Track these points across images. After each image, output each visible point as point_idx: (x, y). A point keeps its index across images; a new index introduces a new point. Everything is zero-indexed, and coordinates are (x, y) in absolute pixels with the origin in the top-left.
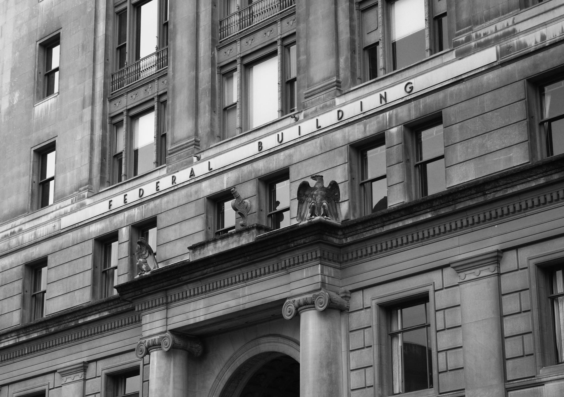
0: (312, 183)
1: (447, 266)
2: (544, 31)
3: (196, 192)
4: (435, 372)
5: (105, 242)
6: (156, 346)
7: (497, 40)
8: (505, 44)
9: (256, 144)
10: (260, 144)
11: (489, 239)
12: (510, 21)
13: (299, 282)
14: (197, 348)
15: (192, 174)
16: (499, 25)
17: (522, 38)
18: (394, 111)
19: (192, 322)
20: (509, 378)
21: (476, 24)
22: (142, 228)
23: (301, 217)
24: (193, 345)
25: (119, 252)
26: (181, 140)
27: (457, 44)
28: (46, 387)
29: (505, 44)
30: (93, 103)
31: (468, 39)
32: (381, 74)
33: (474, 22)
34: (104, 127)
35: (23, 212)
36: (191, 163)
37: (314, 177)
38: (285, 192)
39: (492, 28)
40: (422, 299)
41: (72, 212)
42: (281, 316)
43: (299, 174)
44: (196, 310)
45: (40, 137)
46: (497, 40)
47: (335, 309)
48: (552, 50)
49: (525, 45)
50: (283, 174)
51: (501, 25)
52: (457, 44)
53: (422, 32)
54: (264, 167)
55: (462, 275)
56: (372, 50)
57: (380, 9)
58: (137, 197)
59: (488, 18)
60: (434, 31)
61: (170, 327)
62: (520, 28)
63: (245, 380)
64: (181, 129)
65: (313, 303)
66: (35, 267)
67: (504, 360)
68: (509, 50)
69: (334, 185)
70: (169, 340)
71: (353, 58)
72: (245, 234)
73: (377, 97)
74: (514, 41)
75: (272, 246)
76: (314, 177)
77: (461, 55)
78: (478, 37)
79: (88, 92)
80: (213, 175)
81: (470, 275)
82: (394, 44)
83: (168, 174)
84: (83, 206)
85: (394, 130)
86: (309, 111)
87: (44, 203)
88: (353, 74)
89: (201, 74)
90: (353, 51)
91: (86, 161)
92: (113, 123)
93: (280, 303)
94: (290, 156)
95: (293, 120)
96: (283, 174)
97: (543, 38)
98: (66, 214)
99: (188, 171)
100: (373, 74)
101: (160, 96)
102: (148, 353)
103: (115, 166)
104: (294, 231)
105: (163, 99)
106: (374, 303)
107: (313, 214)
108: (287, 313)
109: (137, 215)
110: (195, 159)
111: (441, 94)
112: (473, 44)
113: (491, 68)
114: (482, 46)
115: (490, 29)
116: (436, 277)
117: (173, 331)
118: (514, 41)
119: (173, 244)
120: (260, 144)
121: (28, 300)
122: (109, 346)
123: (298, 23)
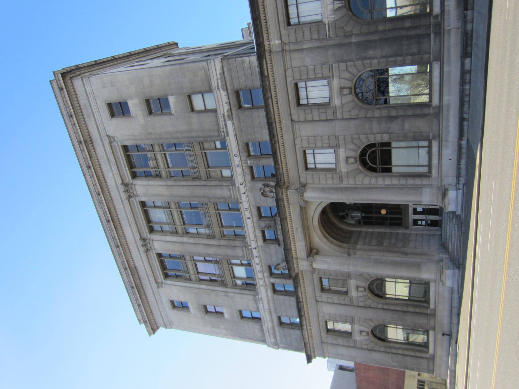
0: (262, 191)
2: (224, 103)
3: (261, 247)
7: (225, 121)
8: (226, 118)
9: (239, 176)
11: (286, 123)
12: (219, 116)
15: (255, 248)
16: (220, 120)
17: (225, 111)
18: (243, 162)
20: (333, 118)
21: (219, 129)
26: (243, 254)
27: (224, 136)
29: (226, 118)
30: (227, 292)
31: (223, 132)
32: (254, 282)
33: (219, 130)
34: (236, 289)
35: (261, 326)
36: (251, 249)
37: (260, 191)
39: (221, 122)
41: (263, 304)
45: (237, 315)
46: (225, 121)
47: (304, 186)
48: (231, 100)
49: (228, 110)
51: (221, 119)
52: (224, 136)
53: (246, 269)
54: (255, 218)
56: (247, 284)
57: (207, 151)
59: (218, 125)
62: (222, 112)
63: (327, 235)
66: (281, 324)
67: (327, 120)
68: (229, 117)
71: (248, 290)
72: (276, 221)
73: (246, 212)
74: (226, 114)
76: (260, 191)
77: (228, 134)
78: (223, 128)
79: (223, 294)
80: (256, 240)
82: (247, 277)
83: (253, 259)
84: (261, 298)
85: (249, 162)
86: (239, 197)
87: (259, 319)
88: (253, 290)
89: (223, 244)
91: (246, 296)
92: (235, 285)
94: (253, 206)
95: (241, 205)
97: (226, 103)
98: (263, 307)
99: (254, 250)
100: (254, 285)
103: (249, 285)
106: (305, 173)
107: (272, 192)
110: (250, 247)
111: (240, 143)
112: (225, 130)
113: (233, 123)
114: (226, 125)
115: (222, 123)
116: (298, 147)
117: (307, 257)
118: (226, 114)
120: (248, 218)
121: (292, 327)
123: (210, 202)
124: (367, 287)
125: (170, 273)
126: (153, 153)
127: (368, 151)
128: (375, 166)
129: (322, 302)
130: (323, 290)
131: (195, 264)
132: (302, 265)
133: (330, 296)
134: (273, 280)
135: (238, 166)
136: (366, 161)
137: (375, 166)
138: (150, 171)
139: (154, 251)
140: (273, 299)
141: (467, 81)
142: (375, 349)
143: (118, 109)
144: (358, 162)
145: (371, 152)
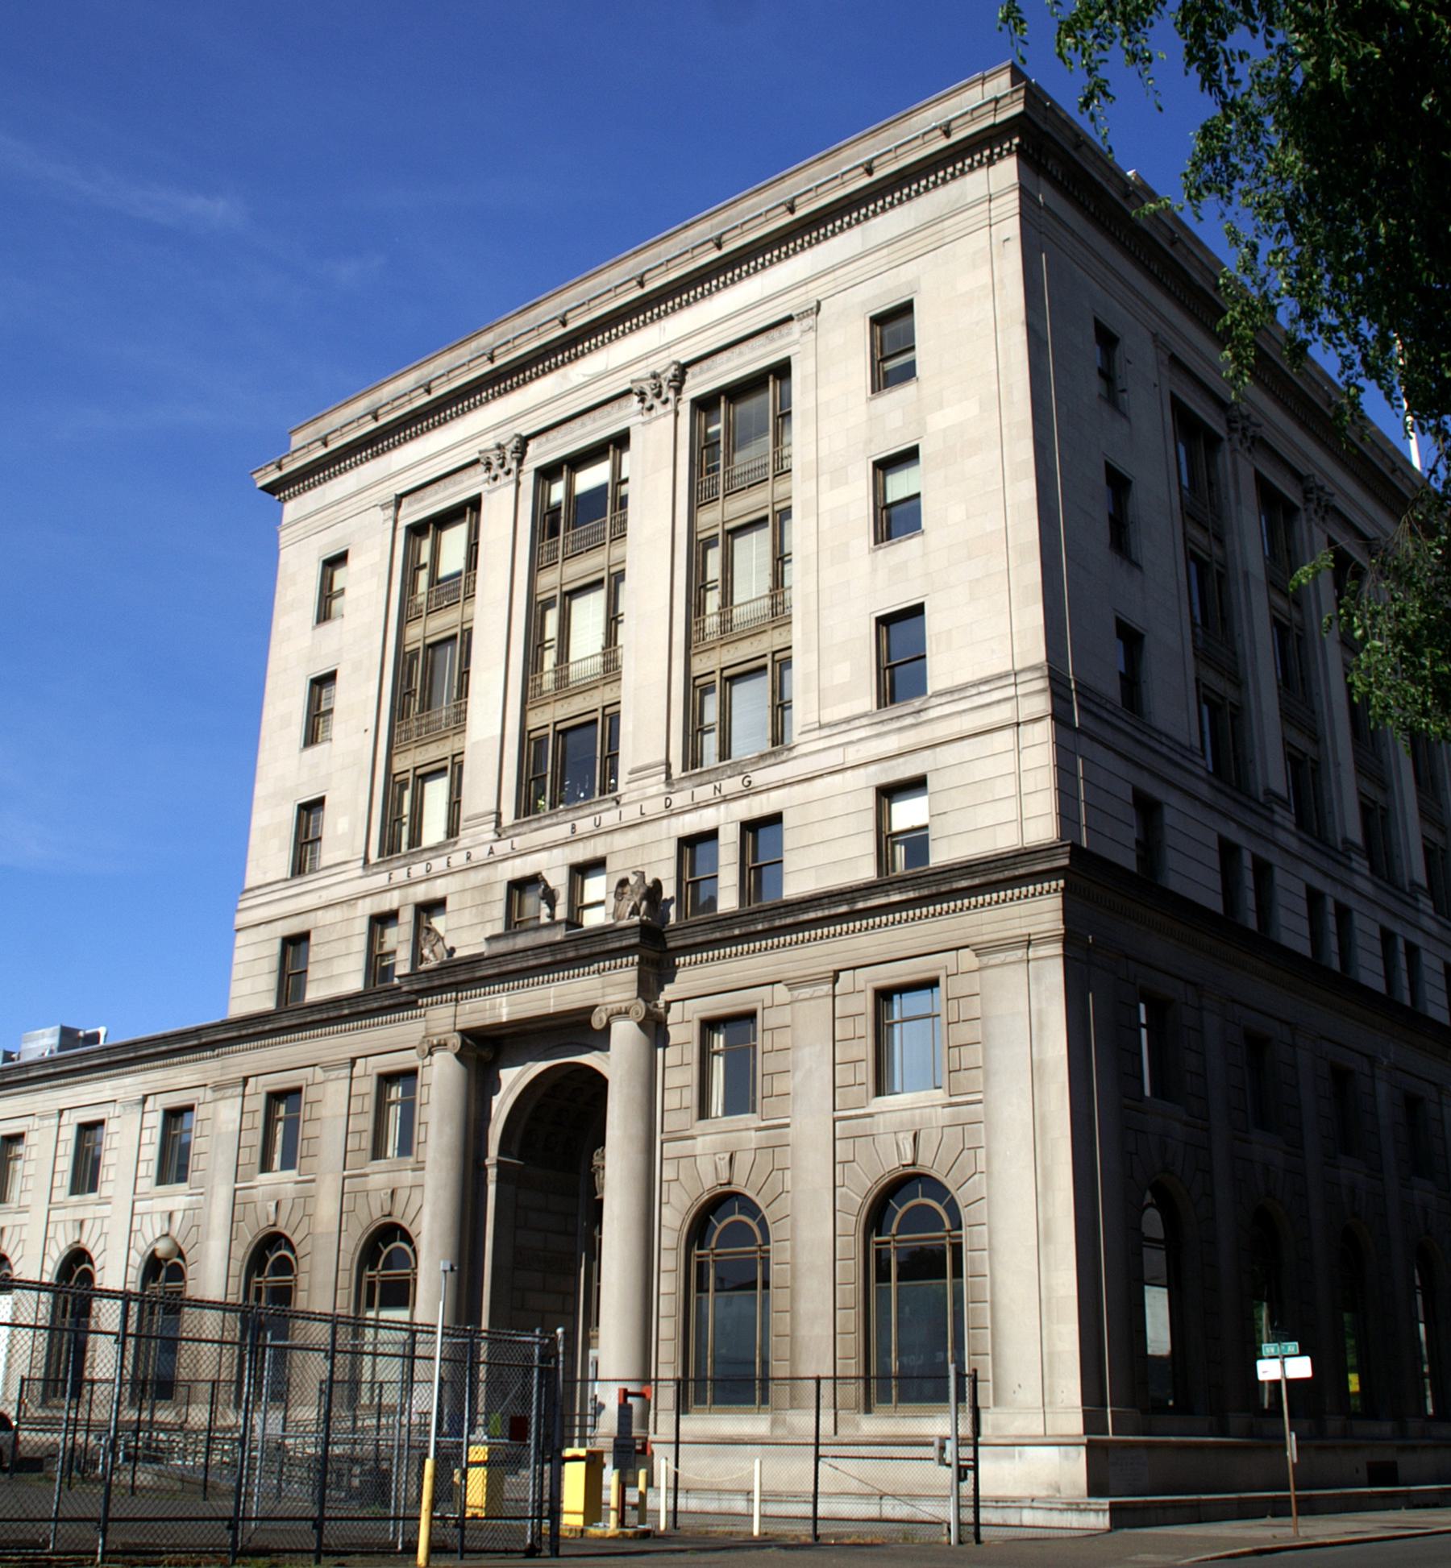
0: (633, 880)
1: (967, 947)
4: (759, 1095)
5: (382, 920)
6: (442, 1045)
10: (574, 827)
13: (609, 988)
14: (487, 1054)
19: (488, 1022)
22: (435, 906)
23: (616, 915)
24: (485, 1051)
25: (398, 938)
28: (303, 1083)
38: (596, 888)
40: (932, 984)
42: (589, 1022)
43: (618, 867)
44: (502, 1006)
50: (597, 865)
55: (796, 993)
58: (424, 872)
60: (181, 1063)
61: (458, 1027)
64: (479, 795)
65: (627, 1012)
69: (657, 884)
70: (456, 1041)
75: (583, 950)
81: (805, 992)
90: (556, 814)
93: (590, 1009)
96: (597, 865)
101: (454, 756)
102: (431, 1053)
104: (602, 932)
105: (457, 759)
108: (597, 1022)
109: (422, 893)
116: (199, 1092)
119: (467, 932)
120: (574, 827)
122: (391, 1039)
124: (733, 1188)
125: (426, 546)
126: (770, 476)
127: (940, 1203)
128: (894, 1230)
129: (351, 1078)
130: (884, 996)
131: (597, 584)
132: (445, 1017)
133: (369, 1104)
134: (407, 916)
135: (718, 789)
136: (726, 1216)
137: (894, 1230)
138: (605, 515)
139: (486, 486)
140: (487, 886)
141: (299, 1473)
142: (132, 1252)
143: (892, 337)
144: (720, 1190)
145: (746, 1224)
